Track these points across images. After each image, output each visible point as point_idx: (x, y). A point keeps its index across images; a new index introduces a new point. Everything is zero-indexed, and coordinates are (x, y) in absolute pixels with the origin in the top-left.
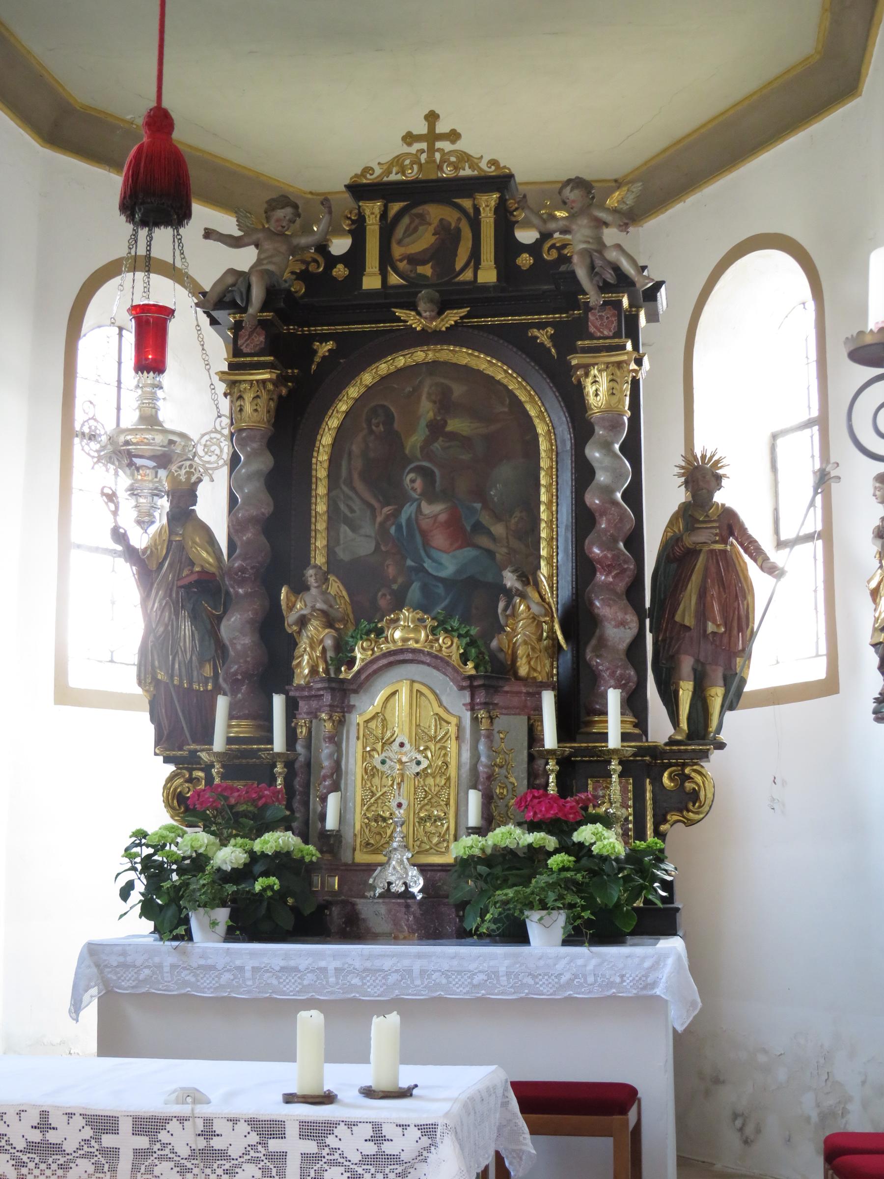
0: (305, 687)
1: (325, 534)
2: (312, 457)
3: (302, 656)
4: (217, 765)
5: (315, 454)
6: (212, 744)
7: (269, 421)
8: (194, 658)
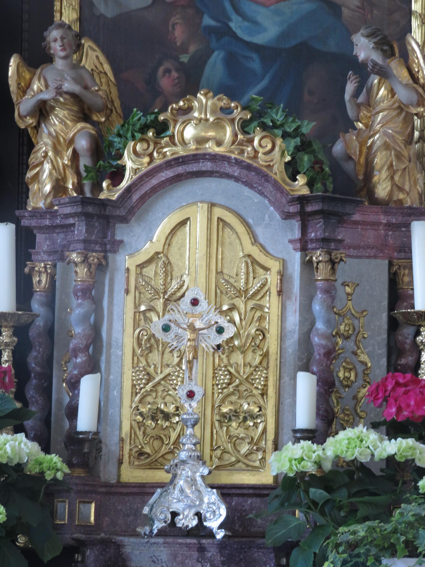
0: (46, 213)
3: (42, 163)
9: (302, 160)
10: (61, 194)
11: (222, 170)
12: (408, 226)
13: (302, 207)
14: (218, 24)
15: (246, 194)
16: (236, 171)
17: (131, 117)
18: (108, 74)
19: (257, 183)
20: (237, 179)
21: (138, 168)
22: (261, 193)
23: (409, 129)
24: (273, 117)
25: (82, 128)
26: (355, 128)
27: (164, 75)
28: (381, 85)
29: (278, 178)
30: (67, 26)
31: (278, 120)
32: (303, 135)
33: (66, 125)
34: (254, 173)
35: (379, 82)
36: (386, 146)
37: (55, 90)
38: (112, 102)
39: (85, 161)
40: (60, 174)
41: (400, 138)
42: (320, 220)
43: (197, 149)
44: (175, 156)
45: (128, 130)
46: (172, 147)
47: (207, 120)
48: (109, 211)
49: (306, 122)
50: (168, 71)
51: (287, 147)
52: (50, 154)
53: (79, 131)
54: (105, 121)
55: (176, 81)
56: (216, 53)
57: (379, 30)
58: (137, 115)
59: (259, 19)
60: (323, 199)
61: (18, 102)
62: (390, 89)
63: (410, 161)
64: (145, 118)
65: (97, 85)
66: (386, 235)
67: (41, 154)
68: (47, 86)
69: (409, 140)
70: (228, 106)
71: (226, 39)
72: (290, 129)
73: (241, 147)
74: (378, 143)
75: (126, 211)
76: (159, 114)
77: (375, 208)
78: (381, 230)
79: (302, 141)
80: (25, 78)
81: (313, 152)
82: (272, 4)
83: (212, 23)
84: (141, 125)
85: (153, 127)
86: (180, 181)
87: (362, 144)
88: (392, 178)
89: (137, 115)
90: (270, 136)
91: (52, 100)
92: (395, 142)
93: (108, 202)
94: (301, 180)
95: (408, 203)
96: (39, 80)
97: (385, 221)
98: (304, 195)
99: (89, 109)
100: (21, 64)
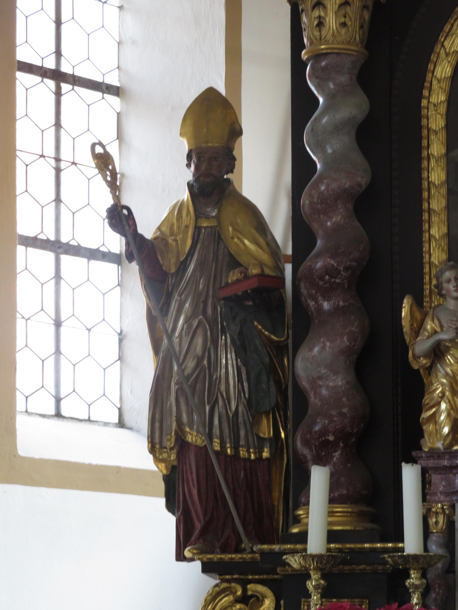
0: (444, 453)
1: (444, 216)
2: (421, 97)
3: (439, 404)
4: (315, 576)
5: (426, 93)
6: (402, 541)
7: (361, 41)
8: (240, 409)
37: (455, 331)
52: (447, 393)
96: (433, 320)
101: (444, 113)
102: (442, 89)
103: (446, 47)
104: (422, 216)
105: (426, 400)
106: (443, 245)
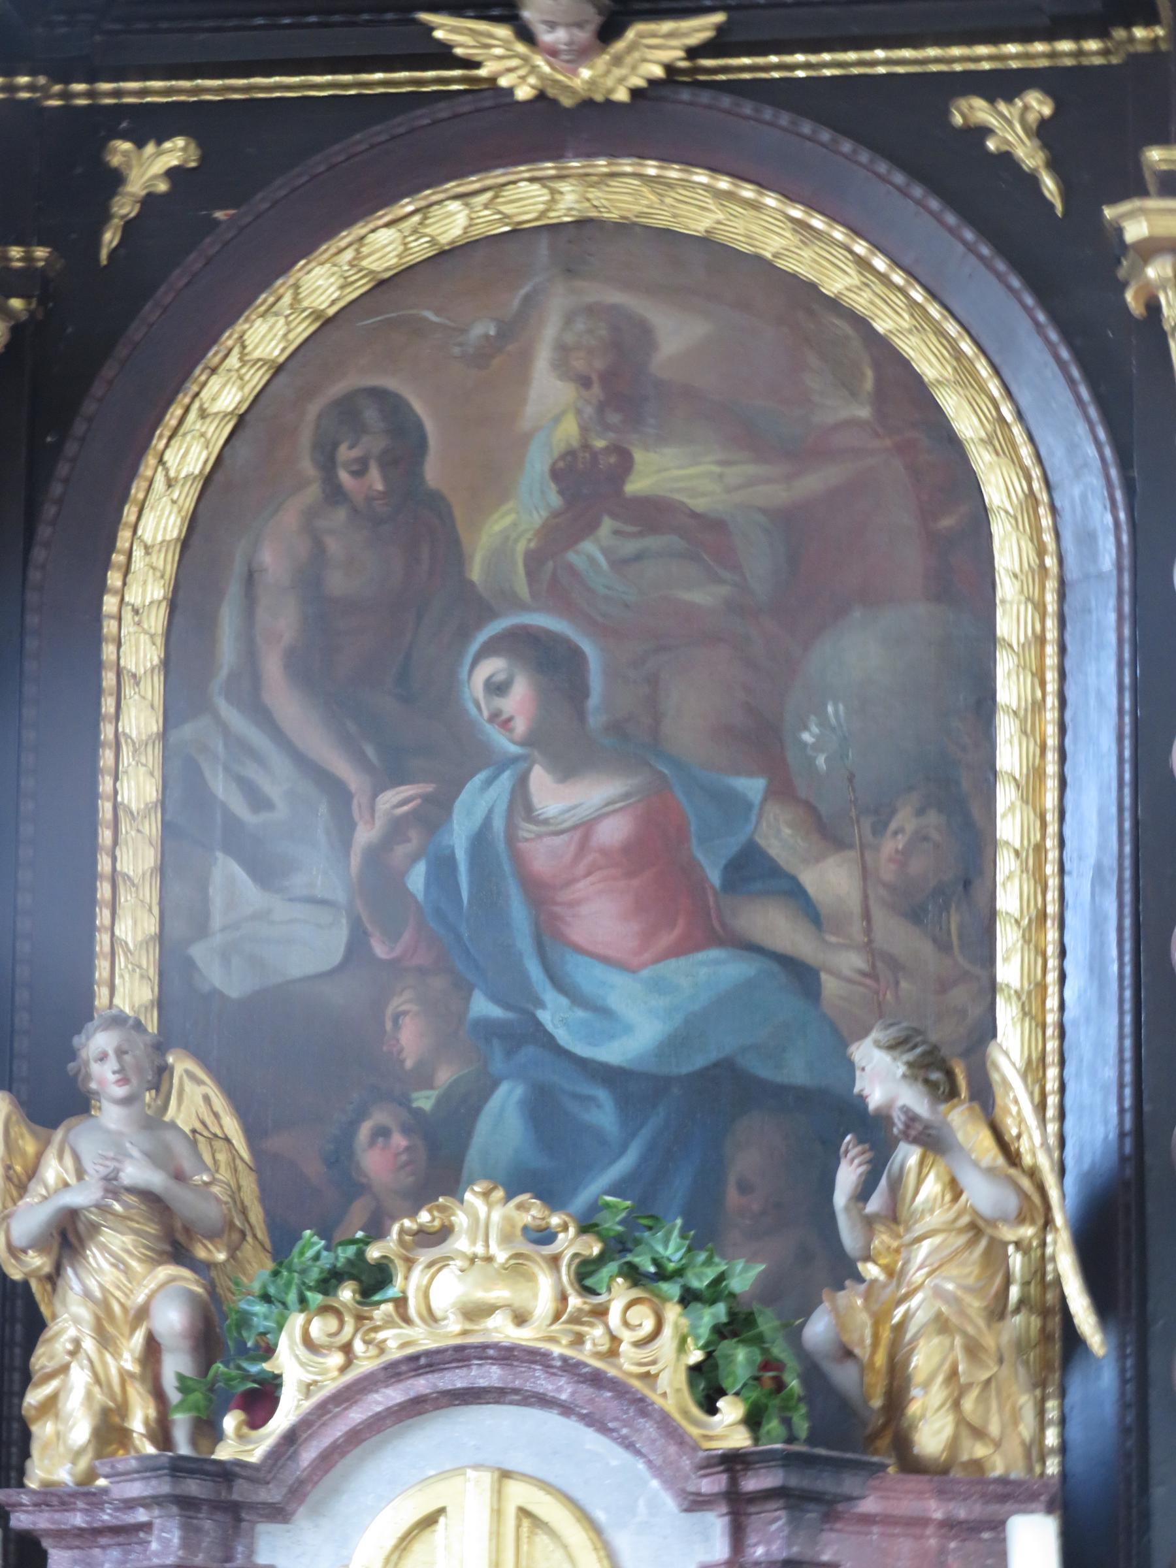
0: (74, 1495)
2: (102, 588)
3: (64, 1369)
5: (114, 579)
9: (730, 1359)
10: (114, 1446)
11: (528, 1386)
12: (998, 1526)
13: (734, 1481)
14: (510, 1015)
15: (588, 1447)
16: (564, 1389)
17: (296, 1251)
18: (234, 1142)
19: (616, 1419)
20: (566, 1410)
21: (315, 1382)
22: (629, 1445)
23: (998, 1280)
24: (657, 1252)
25: (172, 1279)
26: (860, 1279)
27: (372, 1142)
28: (925, 1171)
29: (670, 1405)
30: (131, 1022)
31: (670, 1260)
32: (732, 1295)
33: (127, 1270)
34: (609, 1394)
35: (921, 1163)
36: (941, 1325)
37: (102, 1183)
38: (244, 1212)
39: (176, 1365)
40: (112, 1396)
41: (975, 1305)
42: (778, 1513)
43: (465, 1333)
44: (409, 1351)
45: (288, 1285)
46: (401, 1327)
47: (489, 1259)
48: (241, 1491)
49: (739, 1265)
50: (382, 1132)
51: (694, 1327)
53: (162, 1286)
54: (227, 1261)
55: (404, 1158)
56: (503, 1088)
57: (917, 1032)
58: (311, 1242)
59: (614, 1001)
60: (789, 1460)
61: (6, 1212)
62: (947, 1179)
63: (1001, 1361)
64: (332, 1254)
65: (207, 1169)
66: (943, 1551)
67: (62, 1345)
68: (80, 1173)
69: (998, 1311)
70: (543, 1223)
71: (529, 1052)
72: (701, 1280)
73: (578, 1328)
74: (921, 1318)
75: (284, 1490)
76: (367, 1244)
77: (914, 1482)
78: (929, 1537)
79: (732, 1314)
80: (23, 1154)
81: (758, 1340)
82: (644, 965)
83: (495, 1012)
84: (322, 1271)
85: (353, 1277)
86: (420, 1414)
87: (879, 1319)
88: (956, 1405)
89: (311, 1242)
90: (649, 1300)
91: (93, 1209)
92: (962, 1313)
93: (237, 1469)
94: (730, 1410)
95: (998, 1468)
96: (60, 1157)
97: (938, 1515)
98: (739, 1449)
99: (187, 1230)
100: (14, 1118)
101: (160, 631)
102: (154, 569)
103: (169, 464)
104: (95, 890)
105: (41, 1360)
106: (144, 964)
